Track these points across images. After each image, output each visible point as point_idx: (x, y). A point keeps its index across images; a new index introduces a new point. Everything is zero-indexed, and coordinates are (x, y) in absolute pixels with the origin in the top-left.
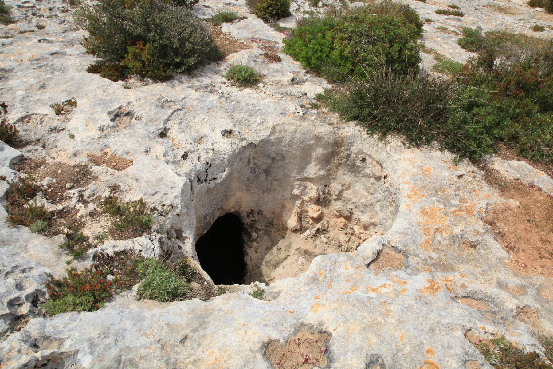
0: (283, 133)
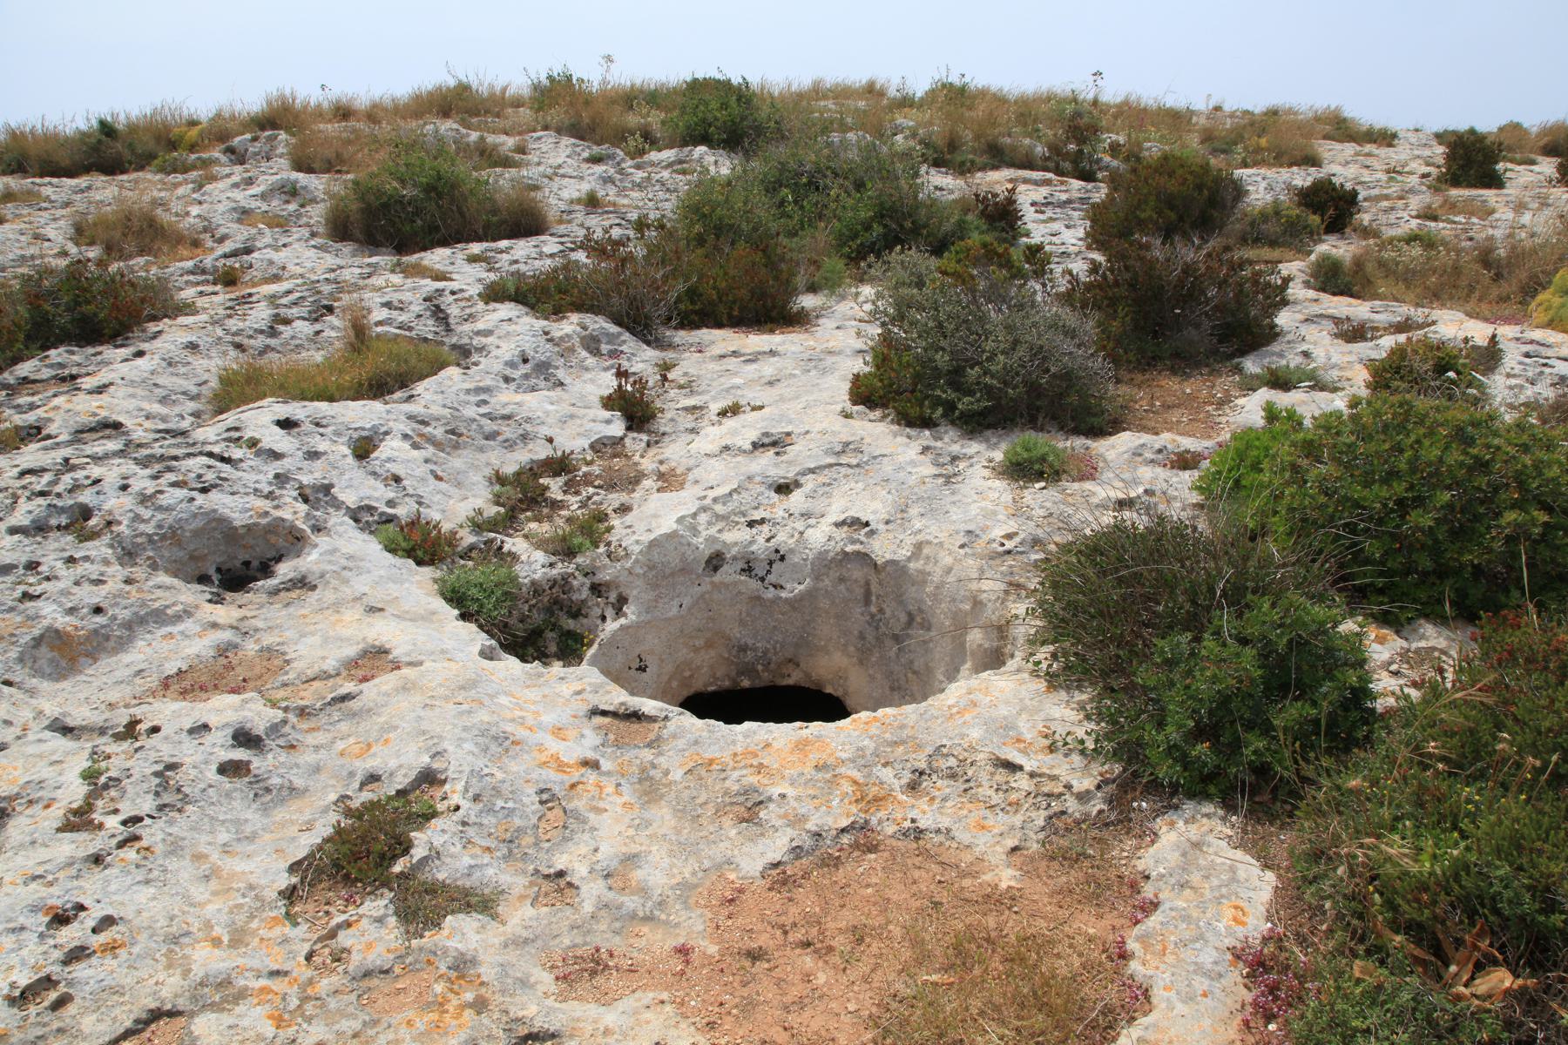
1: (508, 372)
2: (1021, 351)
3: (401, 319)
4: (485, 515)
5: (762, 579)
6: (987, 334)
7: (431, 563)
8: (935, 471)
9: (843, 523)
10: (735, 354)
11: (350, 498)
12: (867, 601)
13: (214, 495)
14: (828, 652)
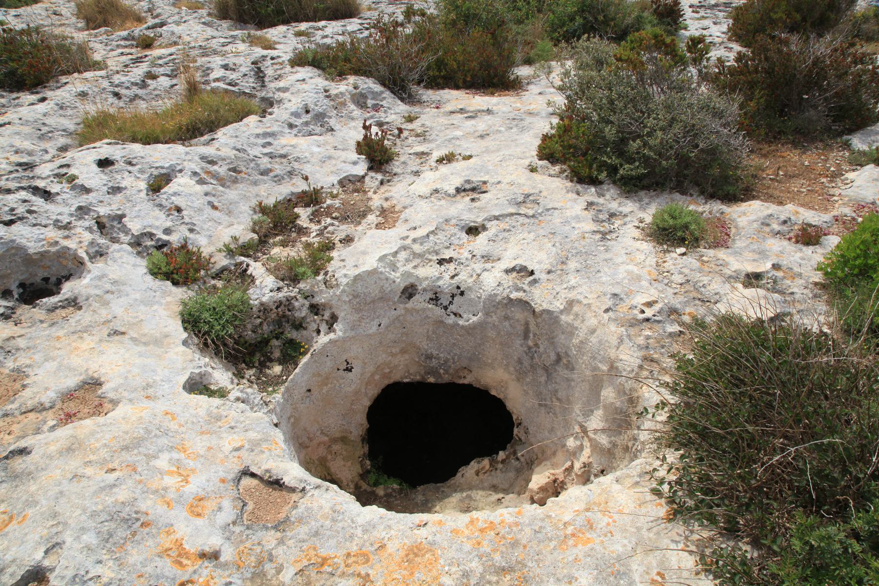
0: (579, 321)
1: (293, 120)
2: (677, 129)
3: (231, 77)
4: (241, 241)
5: (446, 308)
6: (650, 112)
7: (185, 283)
8: (593, 227)
9: (513, 269)
10: (462, 111)
11: (135, 226)
12: (526, 336)
13: (16, 228)
14: (493, 368)
